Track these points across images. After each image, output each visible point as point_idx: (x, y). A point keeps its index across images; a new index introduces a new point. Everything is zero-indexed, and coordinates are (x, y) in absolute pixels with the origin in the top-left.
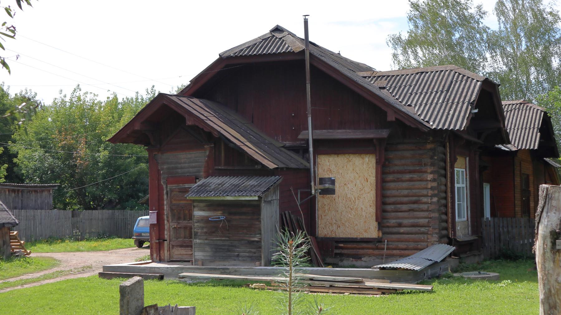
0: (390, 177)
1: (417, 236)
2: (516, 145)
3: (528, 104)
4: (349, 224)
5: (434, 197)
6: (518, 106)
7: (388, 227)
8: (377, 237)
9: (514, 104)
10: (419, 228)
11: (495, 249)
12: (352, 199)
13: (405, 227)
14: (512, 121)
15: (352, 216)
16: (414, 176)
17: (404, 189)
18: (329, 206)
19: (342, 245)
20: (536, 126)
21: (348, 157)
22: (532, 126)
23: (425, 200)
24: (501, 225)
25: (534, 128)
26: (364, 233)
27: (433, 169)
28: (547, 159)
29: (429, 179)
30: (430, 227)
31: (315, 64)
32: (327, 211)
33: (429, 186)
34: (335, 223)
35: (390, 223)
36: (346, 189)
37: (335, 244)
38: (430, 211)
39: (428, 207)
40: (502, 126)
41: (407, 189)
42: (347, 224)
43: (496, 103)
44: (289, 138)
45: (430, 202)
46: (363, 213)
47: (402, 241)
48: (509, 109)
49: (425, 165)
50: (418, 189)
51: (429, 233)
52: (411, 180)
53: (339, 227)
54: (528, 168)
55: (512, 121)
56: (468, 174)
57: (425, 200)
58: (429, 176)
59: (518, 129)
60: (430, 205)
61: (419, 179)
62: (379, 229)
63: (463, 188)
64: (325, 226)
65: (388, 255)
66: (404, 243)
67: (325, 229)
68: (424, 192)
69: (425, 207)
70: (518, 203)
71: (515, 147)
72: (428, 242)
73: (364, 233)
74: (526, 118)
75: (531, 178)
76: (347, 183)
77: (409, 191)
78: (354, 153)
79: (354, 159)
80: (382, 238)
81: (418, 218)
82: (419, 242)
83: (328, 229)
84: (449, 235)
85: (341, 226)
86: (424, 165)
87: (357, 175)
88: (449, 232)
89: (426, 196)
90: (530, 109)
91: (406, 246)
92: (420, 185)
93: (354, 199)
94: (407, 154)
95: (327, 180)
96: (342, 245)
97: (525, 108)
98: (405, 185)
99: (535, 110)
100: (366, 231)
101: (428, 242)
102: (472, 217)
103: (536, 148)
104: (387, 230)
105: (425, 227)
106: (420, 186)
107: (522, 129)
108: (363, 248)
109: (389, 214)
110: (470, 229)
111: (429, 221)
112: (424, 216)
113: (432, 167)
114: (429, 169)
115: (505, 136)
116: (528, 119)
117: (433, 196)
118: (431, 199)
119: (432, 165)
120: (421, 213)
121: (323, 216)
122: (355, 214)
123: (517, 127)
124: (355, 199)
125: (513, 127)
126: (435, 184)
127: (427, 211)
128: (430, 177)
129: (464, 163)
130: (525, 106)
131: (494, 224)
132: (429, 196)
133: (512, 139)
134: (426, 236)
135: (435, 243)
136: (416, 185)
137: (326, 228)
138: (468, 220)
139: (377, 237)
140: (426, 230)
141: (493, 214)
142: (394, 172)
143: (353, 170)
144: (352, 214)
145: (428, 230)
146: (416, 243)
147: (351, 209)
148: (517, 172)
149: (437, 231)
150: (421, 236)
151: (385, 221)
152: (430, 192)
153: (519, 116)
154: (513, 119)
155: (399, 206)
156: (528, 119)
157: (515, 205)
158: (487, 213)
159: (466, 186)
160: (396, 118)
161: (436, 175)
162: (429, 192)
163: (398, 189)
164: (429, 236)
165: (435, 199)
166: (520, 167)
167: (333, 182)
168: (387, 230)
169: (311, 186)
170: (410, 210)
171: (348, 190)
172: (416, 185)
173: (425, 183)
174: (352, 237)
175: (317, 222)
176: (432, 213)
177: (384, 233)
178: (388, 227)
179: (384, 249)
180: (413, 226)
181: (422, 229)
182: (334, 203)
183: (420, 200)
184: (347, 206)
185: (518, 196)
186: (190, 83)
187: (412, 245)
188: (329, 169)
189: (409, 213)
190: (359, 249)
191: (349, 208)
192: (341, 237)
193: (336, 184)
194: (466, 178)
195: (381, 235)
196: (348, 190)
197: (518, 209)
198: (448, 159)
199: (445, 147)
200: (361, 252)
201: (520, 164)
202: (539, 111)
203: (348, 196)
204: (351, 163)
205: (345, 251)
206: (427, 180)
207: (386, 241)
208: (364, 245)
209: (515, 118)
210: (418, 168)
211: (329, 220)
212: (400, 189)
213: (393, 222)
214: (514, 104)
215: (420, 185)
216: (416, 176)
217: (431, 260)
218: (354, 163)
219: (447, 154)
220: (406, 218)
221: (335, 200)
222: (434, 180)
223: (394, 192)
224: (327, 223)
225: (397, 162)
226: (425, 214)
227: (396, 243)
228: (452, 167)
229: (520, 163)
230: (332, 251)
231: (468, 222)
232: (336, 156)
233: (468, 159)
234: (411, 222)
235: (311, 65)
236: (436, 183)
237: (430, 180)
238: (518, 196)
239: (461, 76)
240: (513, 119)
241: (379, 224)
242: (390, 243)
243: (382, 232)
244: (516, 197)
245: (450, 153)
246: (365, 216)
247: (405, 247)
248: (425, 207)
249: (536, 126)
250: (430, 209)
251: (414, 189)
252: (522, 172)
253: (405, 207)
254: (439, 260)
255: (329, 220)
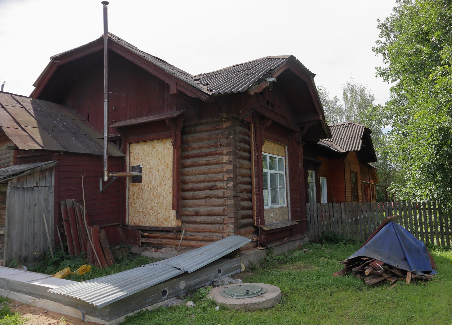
0: (189, 162)
1: (213, 225)
2: (344, 149)
3: (354, 124)
4: (152, 212)
5: (230, 181)
6: (347, 125)
7: (187, 215)
8: (176, 227)
9: (345, 125)
10: (215, 217)
11: (318, 232)
12: (155, 187)
13: (202, 215)
14: (343, 134)
15: (155, 204)
16: (210, 159)
17: (201, 174)
18: (137, 194)
19: (147, 234)
20: (359, 136)
21: (153, 143)
22: (357, 136)
23: (220, 185)
24: (323, 210)
25: (358, 137)
26: (165, 221)
27: (229, 150)
28: (370, 164)
29: (225, 161)
30: (226, 216)
31: (115, 50)
32: (136, 200)
33: (225, 168)
34: (142, 211)
35: (188, 211)
36: (151, 176)
37: (141, 233)
38: (226, 197)
39: (224, 193)
40: (321, 119)
41: (204, 174)
42: (151, 212)
43: (313, 95)
44: (111, 130)
45: (225, 188)
46: (164, 201)
47: (199, 232)
48: (341, 127)
49: (221, 145)
50: (215, 173)
51: (225, 223)
52: (207, 164)
53: (145, 215)
54: (356, 168)
55: (343, 134)
56: (287, 162)
57: (220, 185)
58: (224, 158)
59: (346, 138)
60: (225, 190)
61: (215, 161)
62: (177, 218)
63: (281, 175)
64: (134, 214)
65: (187, 246)
66: (201, 234)
67: (134, 217)
68: (220, 176)
69: (220, 193)
70: (348, 191)
71: (344, 150)
72: (223, 233)
73: (165, 221)
74: (353, 131)
75: (359, 175)
76: (151, 170)
77: (206, 175)
78: (157, 139)
79: (157, 145)
80: (180, 228)
81: (215, 206)
82: (215, 232)
83: (137, 217)
84: (255, 224)
85: (146, 214)
86: (220, 146)
87: (159, 161)
88: (254, 221)
89: (222, 180)
90: (355, 126)
91: (202, 237)
92: (216, 168)
93: (157, 186)
94: (204, 135)
95: (136, 168)
96: (147, 234)
97: (352, 126)
98: (201, 169)
99: (359, 127)
100: (166, 220)
101: (223, 233)
102: (292, 203)
103: (359, 150)
104: (185, 218)
105: (221, 215)
106: (215, 170)
107: (349, 138)
108: (165, 238)
109: (187, 201)
110: (290, 214)
111: (224, 209)
112: (219, 203)
113: (228, 148)
114: (225, 150)
115: (325, 129)
116: (354, 132)
117: (228, 180)
118: (226, 184)
119: (228, 145)
120: (217, 199)
121: (133, 204)
122: (157, 202)
123: (346, 137)
124: (158, 186)
125: (343, 138)
126: (230, 167)
127: (223, 197)
128: (226, 159)
129: (283, 151)
130: (352, 125)
131: (317, 209)
132: (225, 181)
133: (333, 134)
134: (221, 226)
135: (231, 234)
136: (212, 169)
137: (135, 216)
138: (287, 206)
139: (176, 227)
140: (222, 219)
141: (330, 200)
142: (192, 157)
143: (157, 156)
144: (155, 203)
145: (224, 219)
146: (212, 234)
147: (155, 197)
148: (347, 169)
149: (232, 220)
150: (216, 226)
151: (184, 209)
152: (226, 176)
153: (348, 131)
154: (343, 133)
155: (196, 193)
156: (354, 132)
157: (346, 193)
158: (325, 200)
159: (286, 174)
160: (177, 90)
161: (232, 157)
162: (225, 175)
163: (196, 175)
164: (225, 226)
165: (231, 184)
166: (350, 166)
167: (140, 169)
168: (185, 218)
169: (103, 173)
170: (207, 197)
171: (152, 178)
172: (212, 169)
173: (221, 166)
174: (155, 226)
175: (127, 211)
176: (227, 200)
177: (183, 222)
178: (187, 215)
179: (180, 239)
180: (209, 214)
181: (218, 219)
182: (141, 191)
183: (215, 186)
184: (151, 193)
185: (348, 186)
186: (34, 88)
187: (208, 236)
188: (138, 157)
189: (205, 200)
190: (162, 238)
191: (153, 195)
192: (147, 225)
193: (143, 172)
194: (286, 166)
195: (180, 224)
196: (152, 178)
197: (349, 196)
198: (253, 141)
199: (249, 129)
200: (164, 241)
201: (350, 164)
202: (361, 127)
203: (152, 184)
204: (155, 150)
205: (150, 241)
206: (223, 163)
207: (184, 230)
208: (166, 235)
209: (345, 132)
210: (214, 150)
211: (137, 209)
212: (198, 174)
213: (190, 210)
214: (345, 125)
215: (216, 168)
216: (212, 159)
217: (179, 269)
218: (158, 150)
219: (252, 136)
220: (203, 206)
221: (142, 187)
222: (229, 162)
223: (192, 178)
224: (136, 211)
225: (195, 145)
226: (221, 201)
227: (194, 234)
228: (259, 149)
229: (350, 163)
230: (139, 240)
231: (288, 208)
232: (143, 143)
233: (287, 147)
234: (207, 210)
235: (109, 51)
236: (232, 165)
237: (226, 163)
238: (348, 186)
239: (338, 144)
240: (343, 133)
241: (177, 212)
242: (188, 233)
243: (181, 221)
244: (346, 187)
245: (255, 135)
246: (165, 204)
247: (201, 238)
248: (220, 193)
249: (359, 136)
250: (226, 195)
251: (210, 173)
252: (351, 170)
253: (202, 194)
254: (190, 271)
255: (137, 209)
